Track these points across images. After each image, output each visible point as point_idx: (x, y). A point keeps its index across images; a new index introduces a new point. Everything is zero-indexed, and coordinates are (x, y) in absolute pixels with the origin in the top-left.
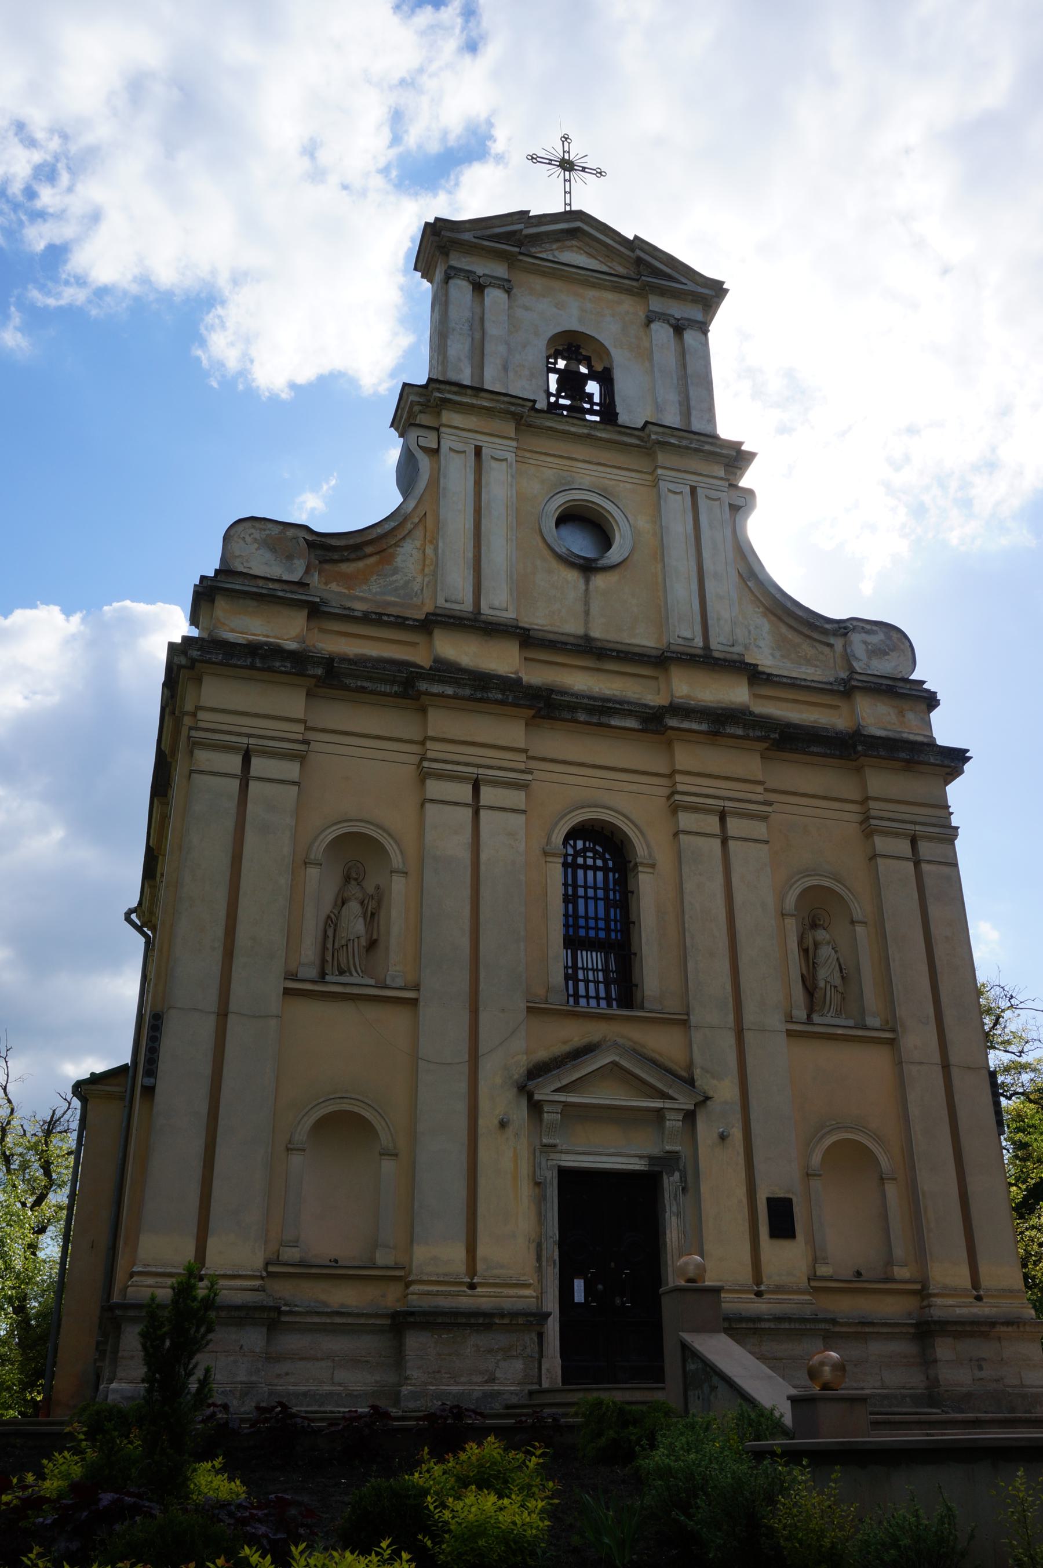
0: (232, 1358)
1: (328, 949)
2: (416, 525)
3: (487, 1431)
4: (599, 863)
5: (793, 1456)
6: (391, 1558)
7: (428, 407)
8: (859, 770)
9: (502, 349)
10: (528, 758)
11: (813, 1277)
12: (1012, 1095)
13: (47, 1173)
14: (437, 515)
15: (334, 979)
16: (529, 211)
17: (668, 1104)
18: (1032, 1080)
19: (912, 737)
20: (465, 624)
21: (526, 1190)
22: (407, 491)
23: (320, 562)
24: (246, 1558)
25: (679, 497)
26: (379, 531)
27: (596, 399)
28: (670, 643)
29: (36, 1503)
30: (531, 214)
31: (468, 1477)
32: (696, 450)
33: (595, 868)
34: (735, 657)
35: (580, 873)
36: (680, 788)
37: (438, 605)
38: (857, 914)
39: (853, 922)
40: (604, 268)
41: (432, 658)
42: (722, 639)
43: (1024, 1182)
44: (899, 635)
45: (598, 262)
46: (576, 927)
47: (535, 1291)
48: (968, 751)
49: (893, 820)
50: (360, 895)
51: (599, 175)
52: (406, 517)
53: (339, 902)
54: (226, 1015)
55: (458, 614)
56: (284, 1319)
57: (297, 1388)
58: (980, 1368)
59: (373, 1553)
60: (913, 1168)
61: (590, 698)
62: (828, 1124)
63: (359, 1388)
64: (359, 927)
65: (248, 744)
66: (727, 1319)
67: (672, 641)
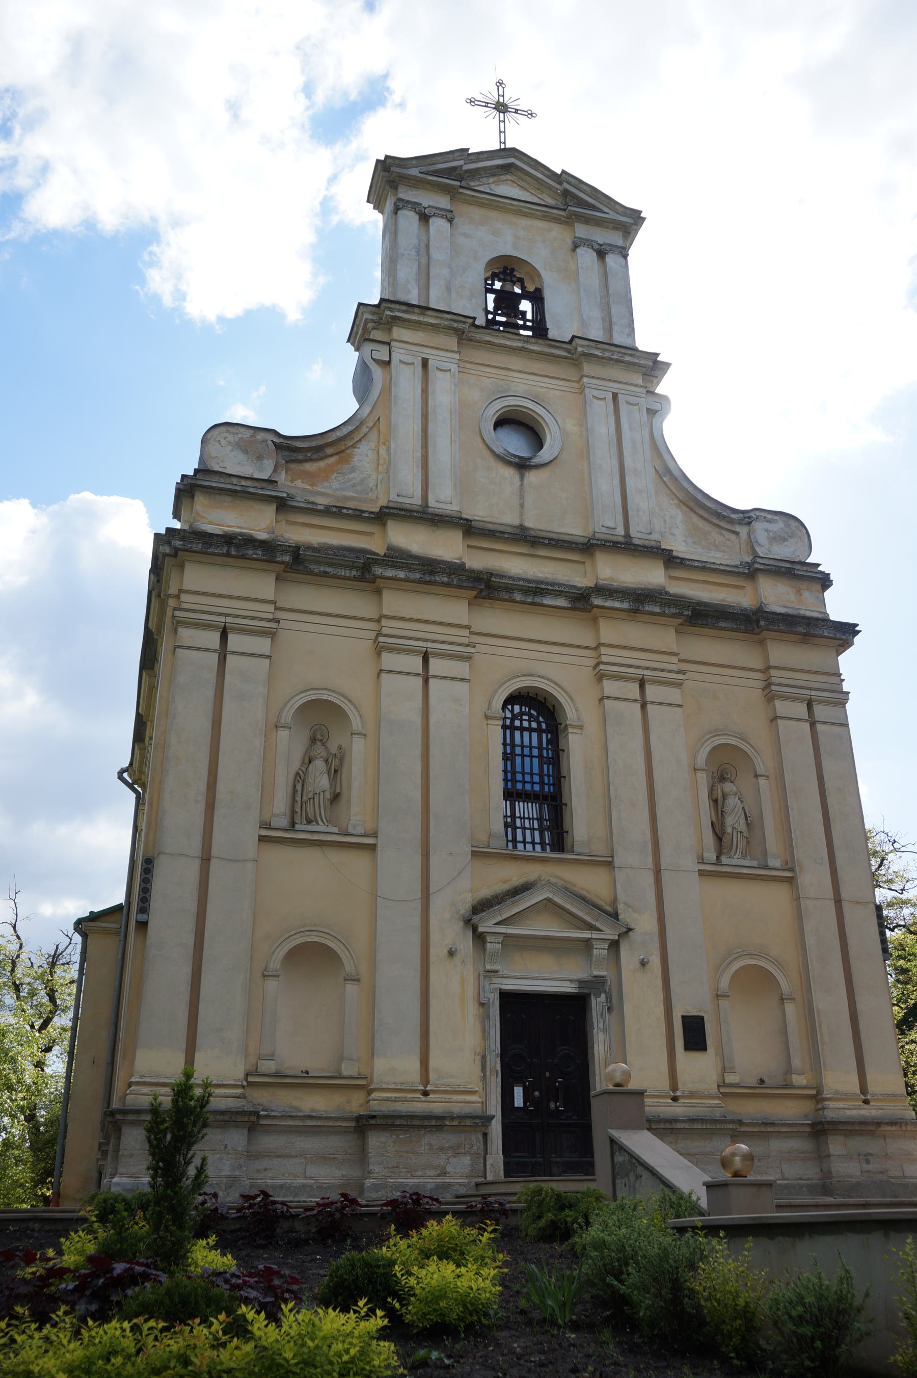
0: (218, 1156)
1: (297, 802)
2: (371, 429)
3: (445, 1213)
4: (534, 725)
5: (712, 1230)
6: (367, 1315)
7: (380, 324)
8: (762, 642)
9: (445, 272)
10: (471, 633)
11: (722, 1084)
12: (895, 927)
13: (52, 999)
15: (303, 827)
17: (595, 935)
18: (912, 914)
19: (808, 614)
20: (414, 516)
21: (472, 1009)
22: (362, 398)
23: (287, 462)
24: (243, 1316)
25: (602, 402)
26: (339, 434)
27: (529, 316)
29: (60, 1273)
30: (470, 152)
31: (429, 1249)
32: (617, 361)
33: (530, 730)
34: (653, 544)
35: (517, 734)
36: (604, 659)
38: (761, 769)
39: (756, 776)
40: (535, 200)
41: (386, 546)
43: (906, 1002)
44: (797, 524)
46: (514, 781)
47: (480, 1097)
48: (857, 625)
49: (791, 686)
50: (324, 754)
51: (530, 116)
52: (362, 422)
53: (307, 761)
54: (209, 860)
55: (408, 507)
56: (263, 1122)
57: (275, 1181)
58: (868, 1162)
59: (352, 1311)
60: (809, 990)
61: (525, 580)
62: (735, 952)
63: (328, 1181)
64: (324, 782)
66: (649, 1121)
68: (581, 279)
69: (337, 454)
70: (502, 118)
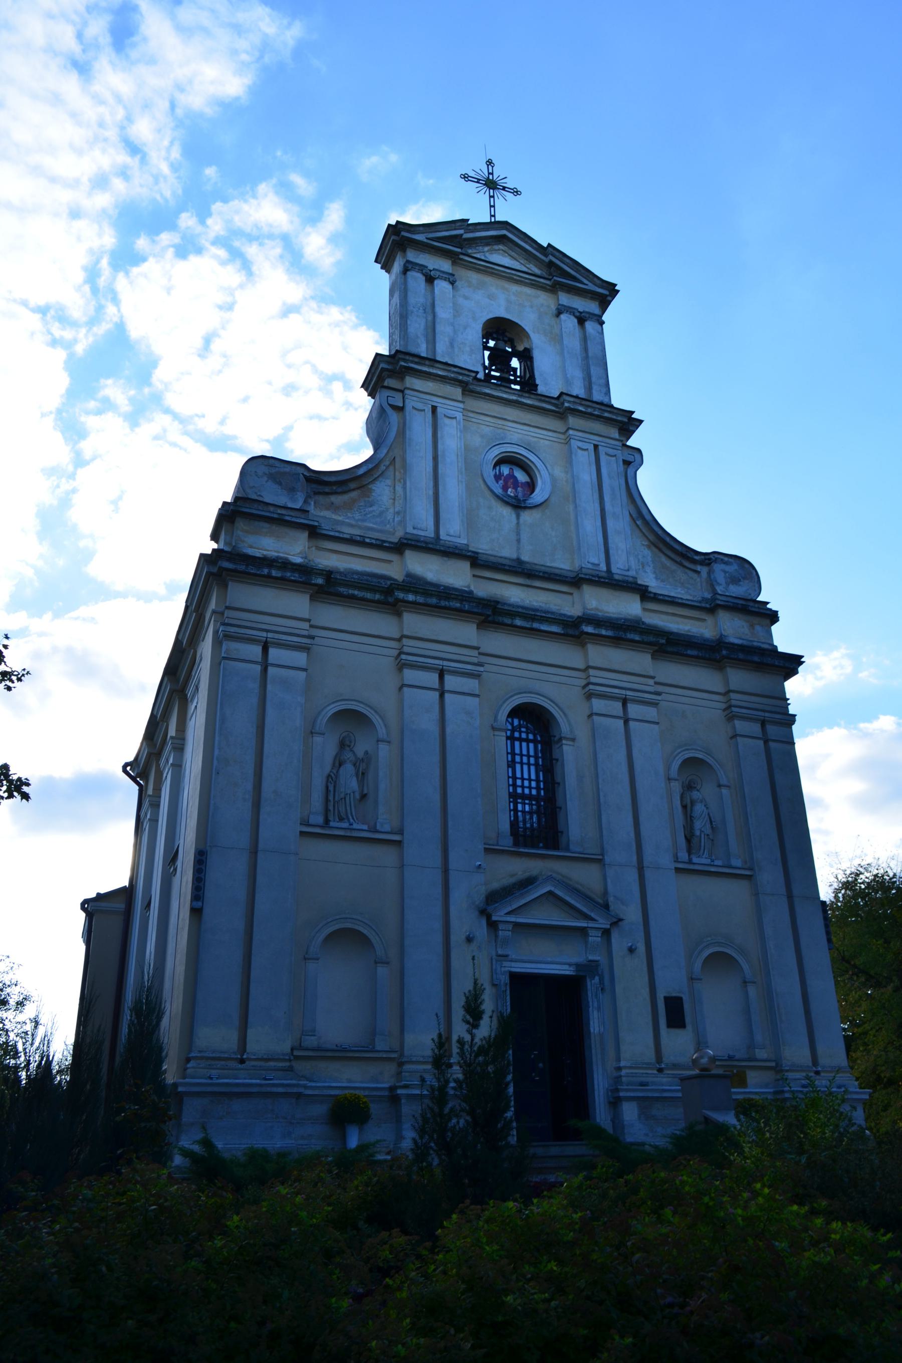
2: (388, 467)
4: (531, 737)
9: (449, 330)
10: (480, 654)
14: (404, 460)
16: (468, 220)
25: (586, 453)
28: (582, 568)
32: (598, 416)
33: (528, 741)
34: (631, 579)
35: (517, 744)
37: (407, 531)
41: (404, 573)
42: (620, 565)
45: (519, 263)
46: (515, 785)
48: (802, 657)
53: (337, 764)
61: (523, 607)
64: (354, 784)
65: (267, 638)
67: (583, 566)
68: (565, 343)
69: (358, 488)
70: (492, 194)
